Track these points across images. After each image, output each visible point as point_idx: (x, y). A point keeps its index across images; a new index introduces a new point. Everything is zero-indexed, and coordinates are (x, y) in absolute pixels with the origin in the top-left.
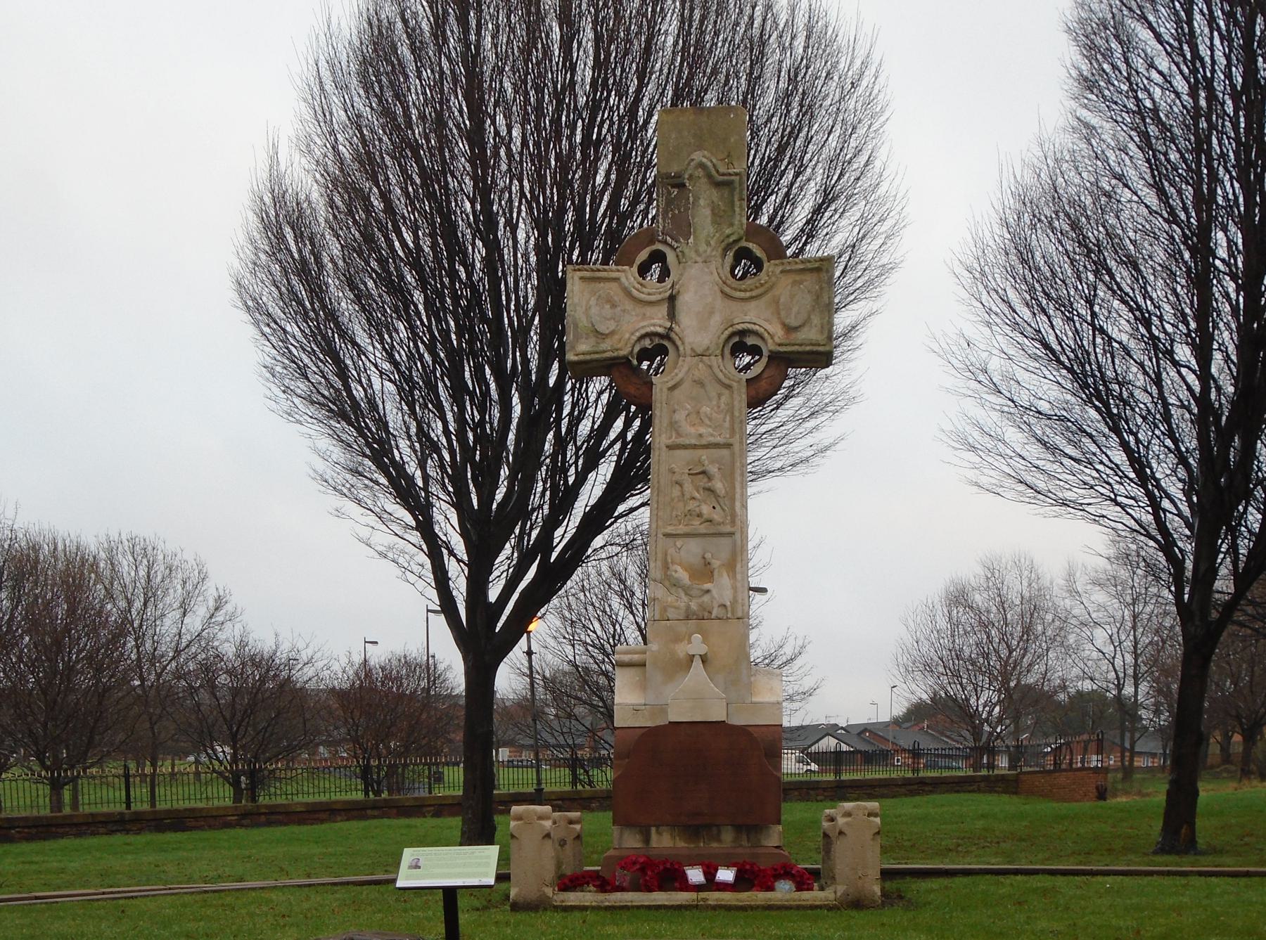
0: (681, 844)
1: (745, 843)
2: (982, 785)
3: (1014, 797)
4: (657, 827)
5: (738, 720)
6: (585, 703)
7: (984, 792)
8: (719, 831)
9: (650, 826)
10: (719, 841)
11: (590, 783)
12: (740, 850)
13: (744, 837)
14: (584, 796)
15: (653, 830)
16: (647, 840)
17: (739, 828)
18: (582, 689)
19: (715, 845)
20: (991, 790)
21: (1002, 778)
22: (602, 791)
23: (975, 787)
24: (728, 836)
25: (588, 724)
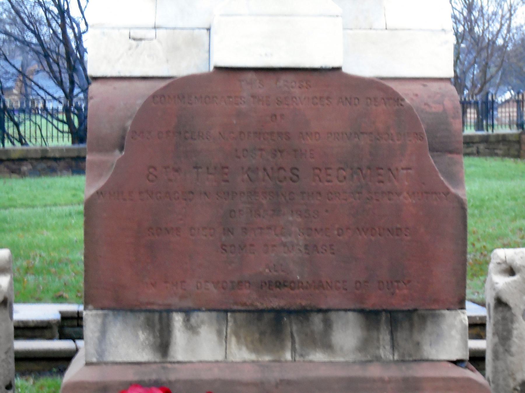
0: (240, 354)
1: (385, 352)
2: (482, 147)
3: (519, 161)
4: (187, 312)
5: (362, 65)
6: (16, 39)
7: (484, 155)
8: (328, 325)
9: (169, 311)
10: (328, 346)
11: (21, 139)
12: (375, 371)
13: (385, 337)
14: (14, 156)
15: (178, 319)
16: (163, 346)
17: (371, 317)
18: (13, 23)
19: (318, 356)
20: (492, 154)
21: (503, 139)
22: (36, 151)
23: (474, 149)
24: (347, 334)
25: (18, 65)
